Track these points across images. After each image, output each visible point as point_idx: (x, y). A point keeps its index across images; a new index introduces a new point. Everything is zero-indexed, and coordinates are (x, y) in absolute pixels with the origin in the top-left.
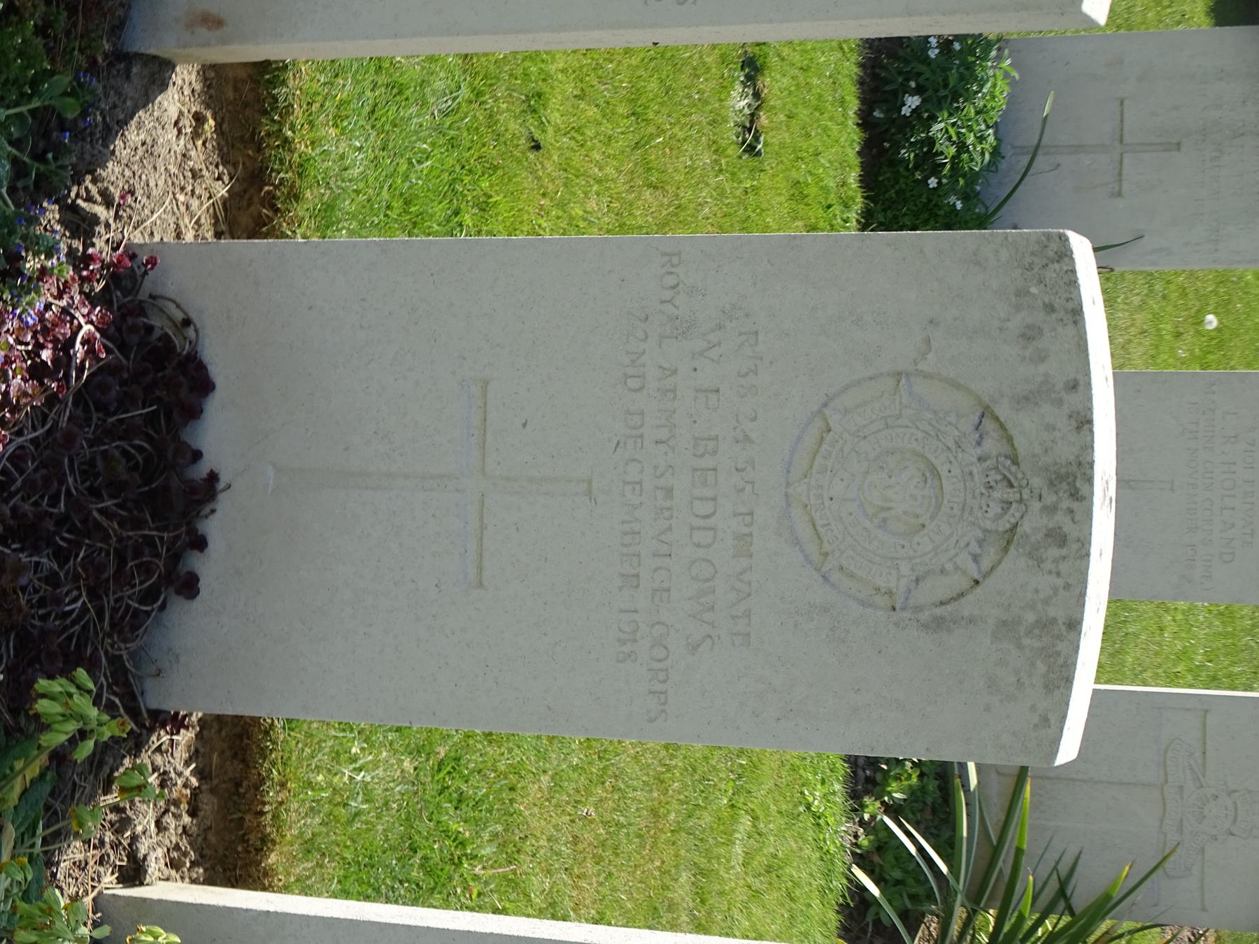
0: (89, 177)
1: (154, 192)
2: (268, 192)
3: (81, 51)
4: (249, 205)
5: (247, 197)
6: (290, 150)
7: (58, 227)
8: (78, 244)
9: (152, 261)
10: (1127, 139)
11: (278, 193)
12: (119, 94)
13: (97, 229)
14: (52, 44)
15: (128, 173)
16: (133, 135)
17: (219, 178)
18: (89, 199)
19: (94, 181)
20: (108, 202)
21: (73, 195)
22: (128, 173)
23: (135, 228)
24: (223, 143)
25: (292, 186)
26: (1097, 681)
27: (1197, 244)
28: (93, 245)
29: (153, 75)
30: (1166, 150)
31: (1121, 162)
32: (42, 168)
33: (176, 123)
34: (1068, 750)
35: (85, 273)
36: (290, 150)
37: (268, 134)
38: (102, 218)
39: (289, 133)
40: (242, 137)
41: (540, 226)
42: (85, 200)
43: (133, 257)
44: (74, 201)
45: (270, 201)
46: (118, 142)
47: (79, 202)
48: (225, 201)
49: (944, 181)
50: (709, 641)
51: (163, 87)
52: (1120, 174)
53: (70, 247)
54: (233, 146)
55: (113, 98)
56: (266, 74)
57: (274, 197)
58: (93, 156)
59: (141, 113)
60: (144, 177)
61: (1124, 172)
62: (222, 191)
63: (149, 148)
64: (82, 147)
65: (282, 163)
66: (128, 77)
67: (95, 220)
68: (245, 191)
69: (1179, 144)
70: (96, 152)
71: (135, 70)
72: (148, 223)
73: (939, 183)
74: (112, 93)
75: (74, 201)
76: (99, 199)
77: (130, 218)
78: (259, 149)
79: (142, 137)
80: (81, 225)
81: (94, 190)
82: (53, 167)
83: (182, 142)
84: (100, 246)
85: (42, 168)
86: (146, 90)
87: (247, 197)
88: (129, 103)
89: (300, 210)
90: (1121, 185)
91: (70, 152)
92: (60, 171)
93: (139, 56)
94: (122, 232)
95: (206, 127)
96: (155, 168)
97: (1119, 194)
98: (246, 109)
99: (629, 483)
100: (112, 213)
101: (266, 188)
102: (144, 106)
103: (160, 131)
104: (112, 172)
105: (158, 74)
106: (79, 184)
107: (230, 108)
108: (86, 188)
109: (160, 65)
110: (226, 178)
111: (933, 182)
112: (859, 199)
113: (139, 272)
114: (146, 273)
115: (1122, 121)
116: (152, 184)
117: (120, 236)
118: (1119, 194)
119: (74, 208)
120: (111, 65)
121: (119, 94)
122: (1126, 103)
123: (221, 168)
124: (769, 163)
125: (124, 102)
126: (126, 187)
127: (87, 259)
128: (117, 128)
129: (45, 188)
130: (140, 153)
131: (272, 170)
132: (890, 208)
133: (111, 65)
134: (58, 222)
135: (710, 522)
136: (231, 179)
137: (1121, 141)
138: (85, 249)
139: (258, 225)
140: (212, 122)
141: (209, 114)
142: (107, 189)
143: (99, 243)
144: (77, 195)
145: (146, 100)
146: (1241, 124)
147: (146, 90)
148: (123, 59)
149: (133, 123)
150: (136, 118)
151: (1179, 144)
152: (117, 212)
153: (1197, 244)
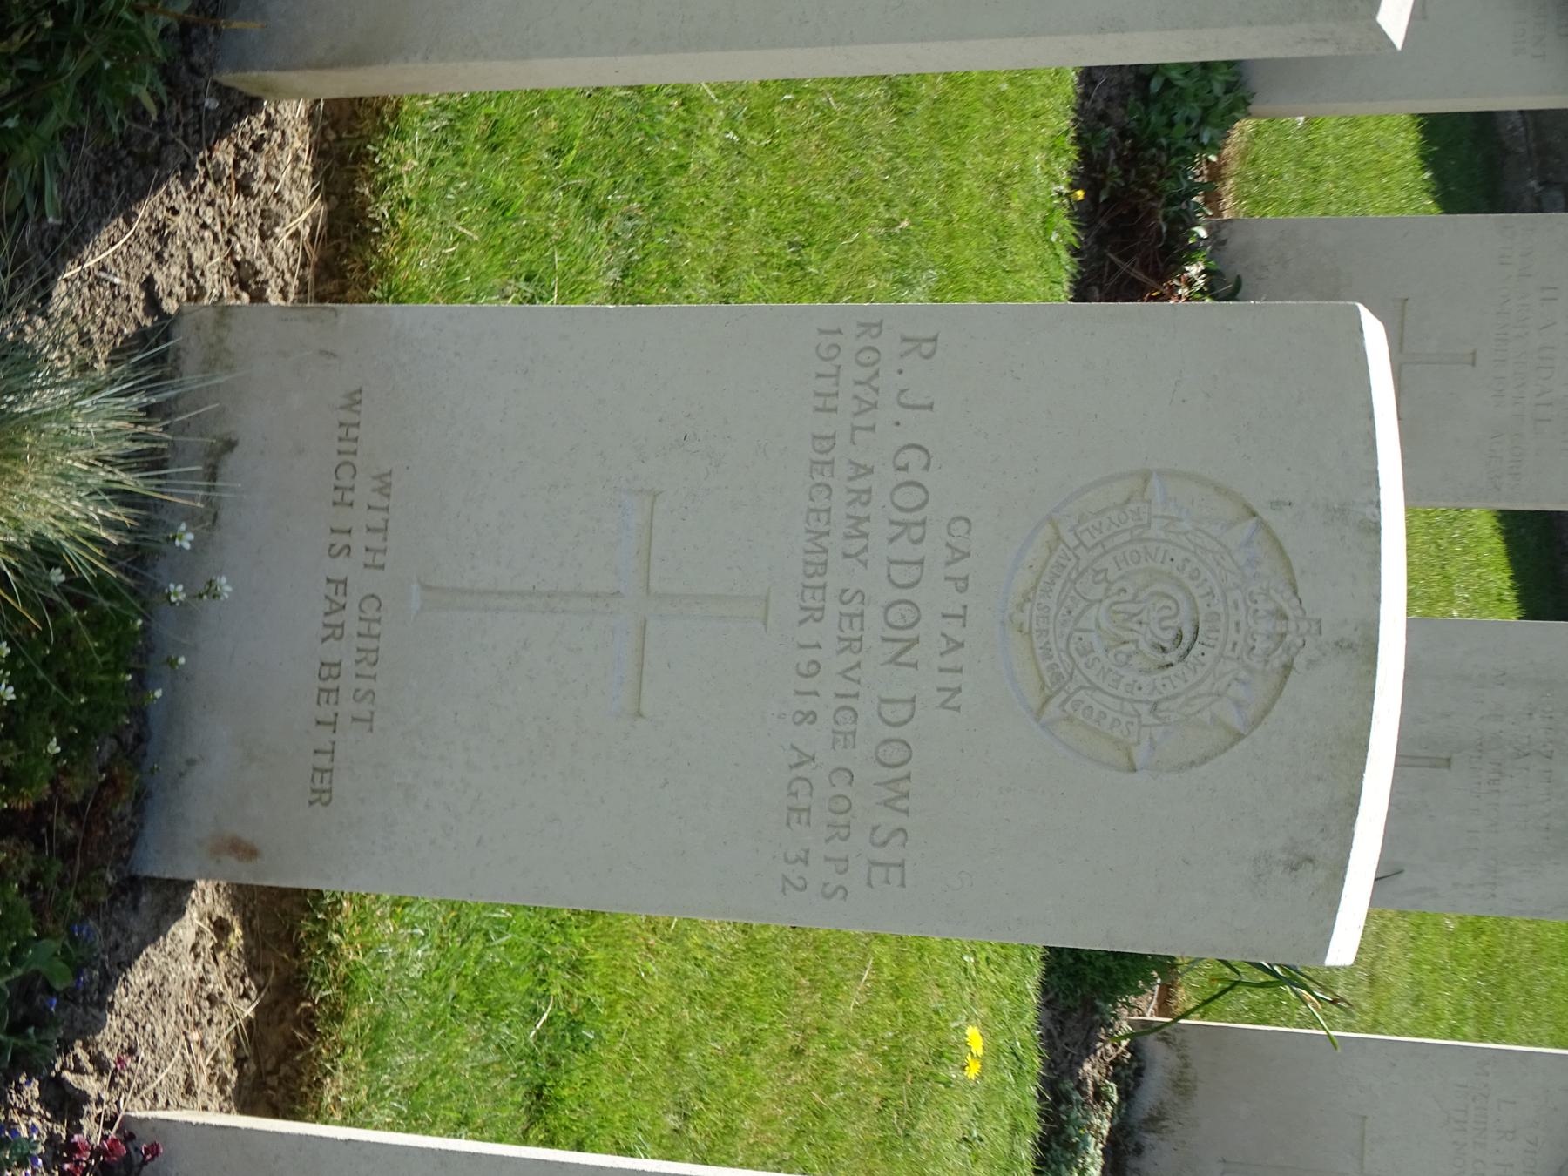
0: (79, 1043)
1: (162, 1043)
2: (306, 1010)
3: (78, 896)
4: (281, 1021)
5: (278, 1010)
6: (335, 957)
7: (36, 1108)
8: (60, 1130)
9: (153, 1150)
11: (317, 1013)
12: (123, 930)
13: (86, 1109)
14: (40, 897)
15: (129, 1025)
16: (138, 977)
17: (245, 995)
18: (79, 1070)
19: (85, 1047)
20: (100, 1064)
21: (58, 1067)
22: (129, 1025)
23: (135, 1094)
24: (252, 943)
25: (335, 1005)
27: (1471, 886)
28: (79, 1129)
29: (166, 901)
30: (1434, 766)
32: (20, 1043)
33: (194, 947)
35: (67, 1166)
36: (335, 957)
37: (309, 936)
38: (93, 1096)
39: (336, 937)
40: (276, 935)
41: (647, 973)
42: (72, 1072)
43: (129, 1137)
44: (58, 1074)
45: (308, 1022)
46: (120, 991)
47: (66, 1074)
48: (250, 1023)
50: (901, 836)
51: (180, 912)
53: (50, 1133)
54: (264, 945)
55: (115, 935)
56: (306, 902)
57: (312, 1016)
58: (84, 1023)
59: (149, 949)
60: (149, 1027)
62: (247, 1010)
63: (157, 991)
64: (73, 1011)
65: (324, 974)
66: (135, 908)
67: (84, 1097)
68: (277, 1003)
69: (1448, 760)
70: (89, 1018)
71: (144, 900)
72: (151, 1087)
74: (114, 929)
75: (58, 1074)
76: (90, 1068)
77: (130, 1083)
78: (297, 954)
79: (149, 977)
80: (65, 1103)
81: (84, 1057)
82: (34, 1041)
83: (199, 966)
84: (91, 1131)
85: (20, 1043)
86: (158, 922)
87: (278, 1010)
88: (135, 940)
89: (345, 1032)
91: (57, 1025)
92: (44, 1047)
93: (151, 880)
94: (117, 1103)
95: (231, 939)
96: (164, 1011)
98: (283, 936)
100: (106, 1081)
101: (303, 1005)
102: (154, 940)
103: (172, 964)
104: (111, 1034)
105: (173, 898)
106: (66, 1053)
107: (264, 898)
108: (75, 1057)
109: (176, 889)
110: (253, 994)
113: (137, 1159)
114: (144, 1162)
116: (158, 1034)
117: (114, 1108)
119: (59, 1081)
120: (114, 898)
121: (123, 930)
123: (247, 981)
125: (129, 938)
126: (126, 1045)
127: (72, 1148)
128: (117, 971)
129: (26, 1063)
130: (145, 997)
131: (312, 982)
133: (114, 898)
134: (38, 1101)
135: (904, 732)
136: (260, 990)
138: (69, 1136)
139: (290, 1046)
140: (238, 932)
141: (236, 924)
142: (101, 1053)
143: (87, 1124)
144: (63, 1067)
145: (157, 931)
146: (1526, 741)
147: (158, 922)
148: (132, 885)
149: (139, 963)
150: (142, 957)
151: (1448, 760)
152: (113, 1078)
153: (1471, 886)
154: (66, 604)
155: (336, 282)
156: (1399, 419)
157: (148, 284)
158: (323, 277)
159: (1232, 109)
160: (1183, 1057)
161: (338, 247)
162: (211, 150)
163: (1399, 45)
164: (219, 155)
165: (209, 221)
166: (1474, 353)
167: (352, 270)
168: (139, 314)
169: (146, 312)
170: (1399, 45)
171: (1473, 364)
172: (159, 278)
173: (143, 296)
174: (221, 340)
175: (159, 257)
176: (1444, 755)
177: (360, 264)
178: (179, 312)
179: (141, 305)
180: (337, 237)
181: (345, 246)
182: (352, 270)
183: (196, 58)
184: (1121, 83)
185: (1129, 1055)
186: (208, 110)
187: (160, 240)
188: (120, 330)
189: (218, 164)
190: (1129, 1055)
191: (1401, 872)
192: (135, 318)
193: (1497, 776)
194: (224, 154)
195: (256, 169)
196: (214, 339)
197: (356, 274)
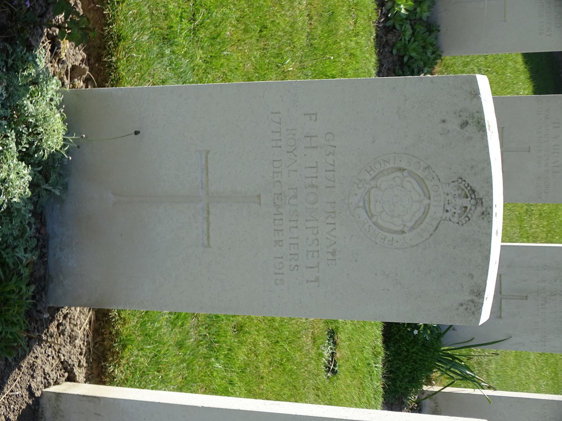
10: (504, 293)
26: (502, 242)
30: (521, 299)
31: (501, 303)
34: (485, 315)
49: (421, 332)
52: (500, 308)
61: (503, 307)
73: (419, 332)
90: (501, 313)
97: (500, 317)
99: (309, 251)
111: (416, 332)
112: (383, 354)
115: (501, 284)
118: (500, 317)
122: (502, 276)
124: (341, 375)
132: (396, 343)
137: (501, 293)
146: (554, 290)
154: (46, 34)
155: (100, 337)
156: (503, 172)
157: (29, 388)
158: (96, 335)
159: (435, 59)
160: (436, 403)
161: (100, 324)
162: (48, 328)
163: (480, 324)
164: (51, 330)
165: (50, 354)
166: (529, 147)
167: (106, 334)
168: (27, 400)
169: (29, 398)
170: (480, 324)
171: (529, 151)
172: (33, 385)
173: (28, 393)
174: (58, 406)
175: (32, 376)
176: (525, 295)
177: (108, 332)
178: (42, 394)
179: (27, 397)
180: (100, 320)
181: (102, 324)
182: (106, 334)
183: (39, 308)
184: (393, 61)
185: (416, 405)
186: (45, 318)
187: (32, 370)
188: (20, 408)
189: (51, 333)
190: (416, 405)
191: (511, 337)
192: (26, 402)
193: (544, 302)
194: (53, 329)
195: (66, 328)
196: (55, 405)
197: (108, 335)
